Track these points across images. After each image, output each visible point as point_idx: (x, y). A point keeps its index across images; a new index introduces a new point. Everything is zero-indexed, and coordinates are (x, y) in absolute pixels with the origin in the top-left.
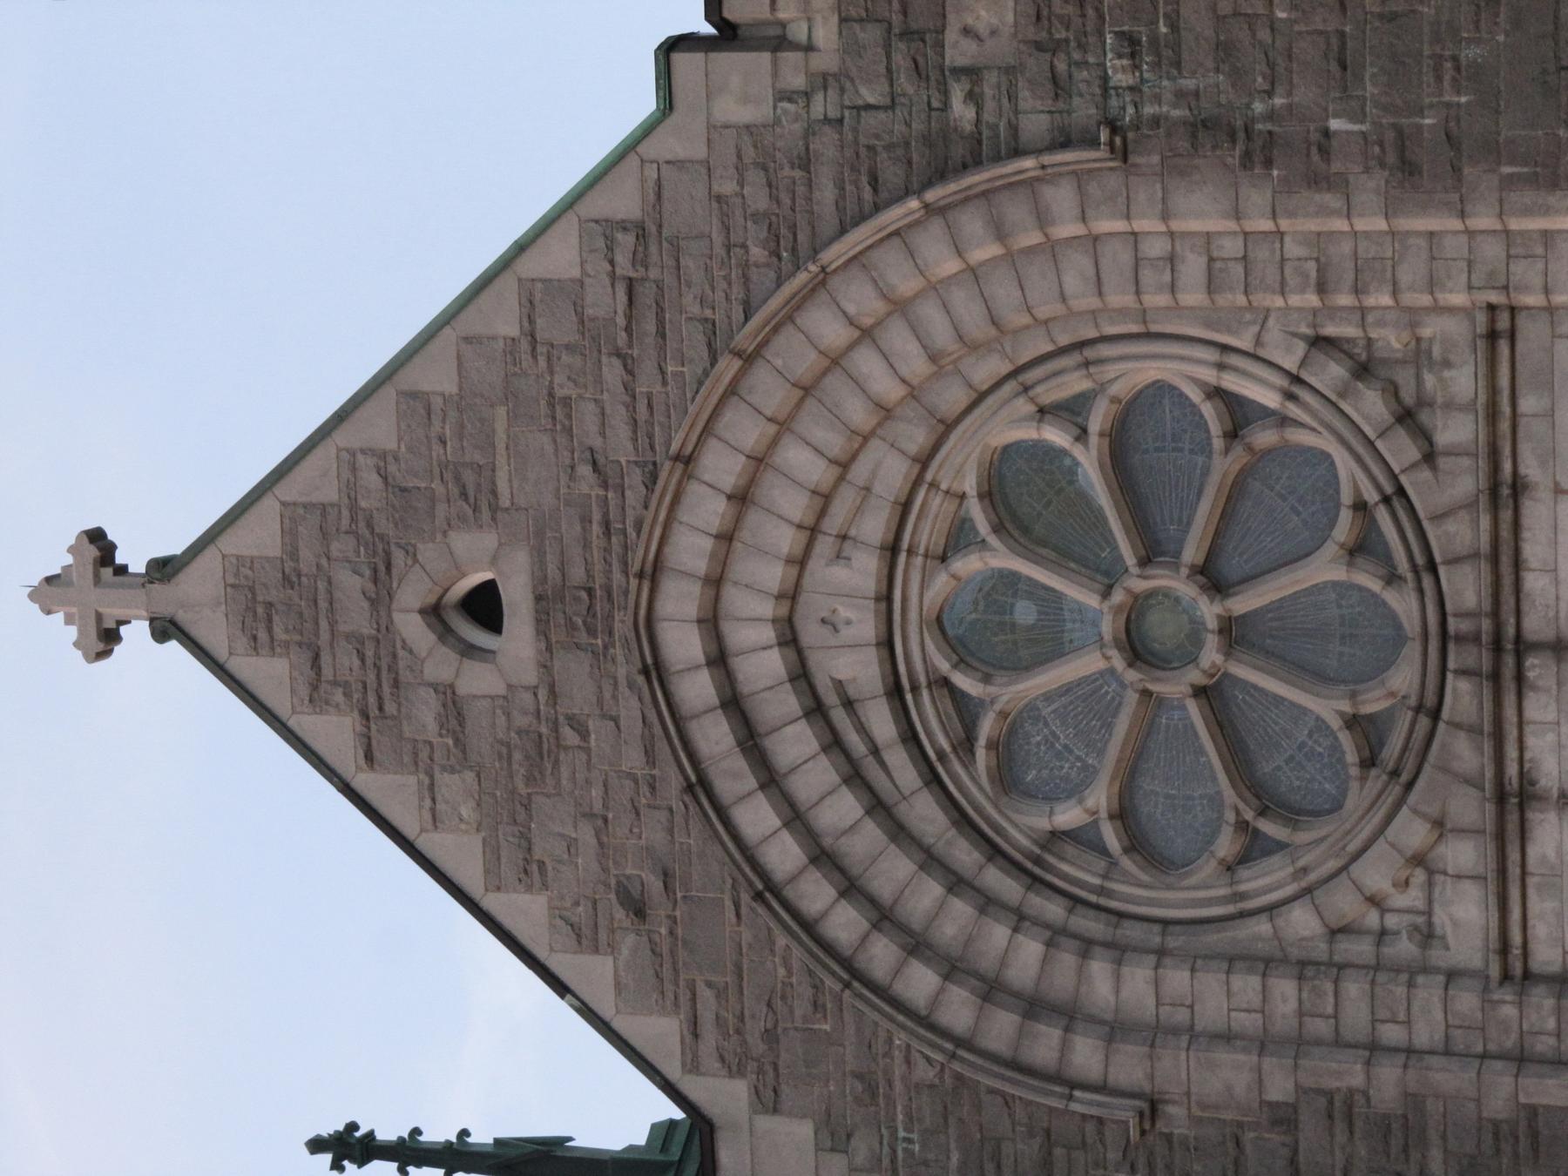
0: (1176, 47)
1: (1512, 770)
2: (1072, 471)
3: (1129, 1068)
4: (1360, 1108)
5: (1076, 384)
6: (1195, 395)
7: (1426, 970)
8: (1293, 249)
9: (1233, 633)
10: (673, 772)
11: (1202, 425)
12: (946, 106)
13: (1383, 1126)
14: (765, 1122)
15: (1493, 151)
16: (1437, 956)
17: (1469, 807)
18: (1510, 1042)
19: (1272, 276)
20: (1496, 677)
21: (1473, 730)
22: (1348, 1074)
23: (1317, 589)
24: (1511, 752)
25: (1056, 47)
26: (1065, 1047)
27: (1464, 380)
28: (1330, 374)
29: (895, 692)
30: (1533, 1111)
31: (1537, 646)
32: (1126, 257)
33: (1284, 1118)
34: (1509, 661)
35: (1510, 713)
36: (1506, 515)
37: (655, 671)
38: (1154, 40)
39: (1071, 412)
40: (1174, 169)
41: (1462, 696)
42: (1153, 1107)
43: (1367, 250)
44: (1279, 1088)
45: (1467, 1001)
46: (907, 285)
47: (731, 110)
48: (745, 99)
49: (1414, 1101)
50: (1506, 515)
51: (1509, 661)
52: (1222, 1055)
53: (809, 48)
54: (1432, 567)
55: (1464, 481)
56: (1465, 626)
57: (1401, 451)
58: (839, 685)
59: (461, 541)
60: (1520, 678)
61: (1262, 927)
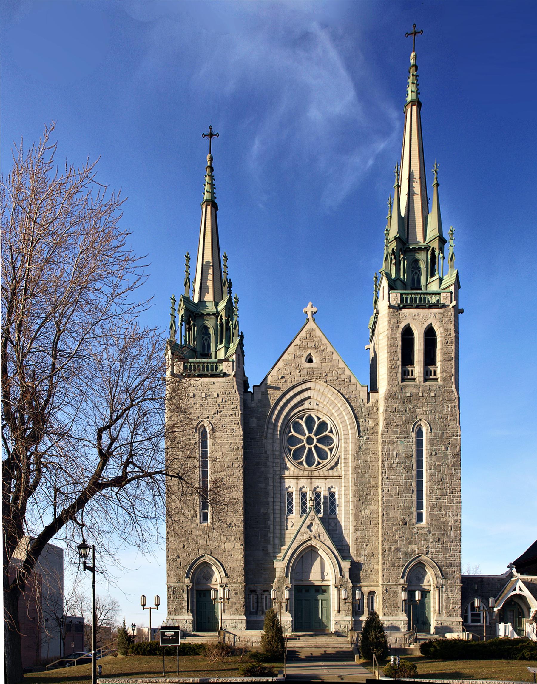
0: (367, 444)
1: (300, 478)
2: (326, 431)
3: (269, 436)
4: (267, 461)
5: (334, 431)
6: (332, 446)
7: (280, 469)
8: (348, 456)
9: (316, 447)
10: (295, 383)
11: (330, 445)
12: (362, 418)
13: (266, 463)
14: (260, 393)
15: (357, 477)
16: (282, 469)
17: (296, 474)
18: (274, 477)
19: (345, 454)
20: (308, 476)
21: (303, 474)
22: (271, 460)
23: (324, 450)
24: (301, 478)
25: (368, 430)
26: (271, 429)
27: (336, 474)
28: (335, 459)
29: (304, 410)
30: (269, 479)
31: (311, 481)
32: (347, 438)
33: (266, 452)
34: (310, 478)
35: (305, 478)
36: (323, 478)
37: (306, 382)
38: (368, 442)
39: (331, 431)
40: (356, 444)
41: (306, 473)
42: (266, 438)
43: (348, 464)
44: (269, 452)
45: (278, 473)
46: (326, 393)
47: (361, 393)
48: (362, 395)
49: (269, 467)
50: (323, 478)
51: (310, 478)
52: (271, 446)
53: (368, 403)
54: (318, 470)
55: (326, 473)
56: (313, 473)
57: (329, 467)
58: (304, 404)
59: (318, 358)
60: (308, 479)
61: (283, 451)
